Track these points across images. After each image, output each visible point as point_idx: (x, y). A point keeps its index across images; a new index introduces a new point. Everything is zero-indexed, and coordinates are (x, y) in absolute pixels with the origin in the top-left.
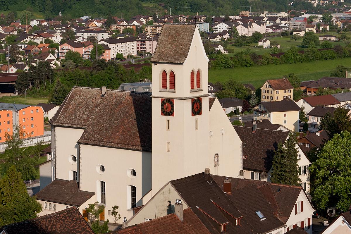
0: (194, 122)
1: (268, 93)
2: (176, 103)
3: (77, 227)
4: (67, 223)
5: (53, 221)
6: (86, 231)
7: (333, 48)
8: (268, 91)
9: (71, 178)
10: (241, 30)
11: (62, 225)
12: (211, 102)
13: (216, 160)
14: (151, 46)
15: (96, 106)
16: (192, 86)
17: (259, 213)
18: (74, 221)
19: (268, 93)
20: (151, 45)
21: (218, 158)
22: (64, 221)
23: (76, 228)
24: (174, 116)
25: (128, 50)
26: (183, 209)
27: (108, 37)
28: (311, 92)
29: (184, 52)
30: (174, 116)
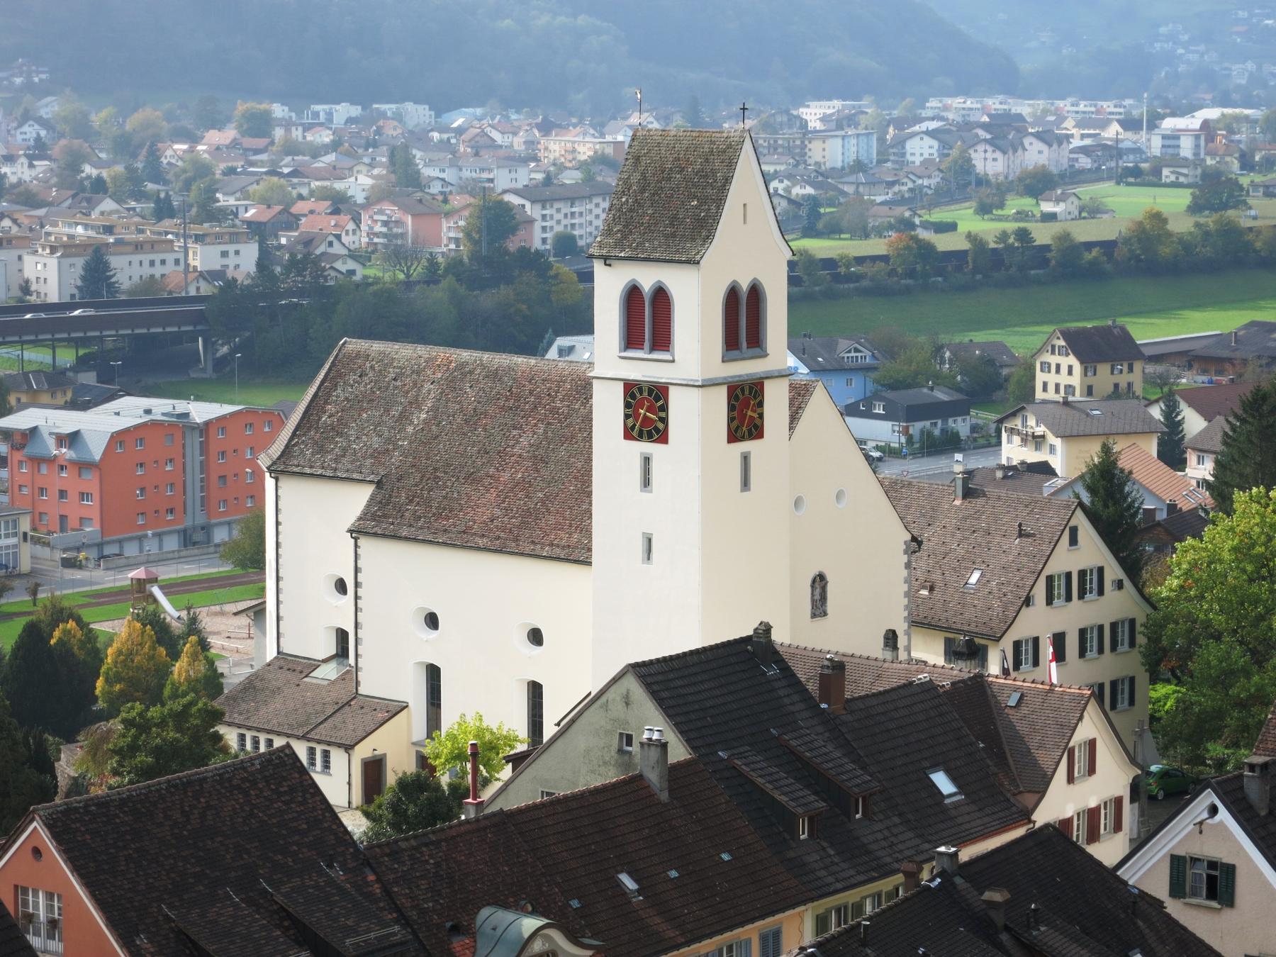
2: (676, 398)
3: (290, 816)
4: (258, 801)
5: (207, 795)
11: (237, 806)
13: (817, 597)
23: (290, 819)
27: (531, 179)
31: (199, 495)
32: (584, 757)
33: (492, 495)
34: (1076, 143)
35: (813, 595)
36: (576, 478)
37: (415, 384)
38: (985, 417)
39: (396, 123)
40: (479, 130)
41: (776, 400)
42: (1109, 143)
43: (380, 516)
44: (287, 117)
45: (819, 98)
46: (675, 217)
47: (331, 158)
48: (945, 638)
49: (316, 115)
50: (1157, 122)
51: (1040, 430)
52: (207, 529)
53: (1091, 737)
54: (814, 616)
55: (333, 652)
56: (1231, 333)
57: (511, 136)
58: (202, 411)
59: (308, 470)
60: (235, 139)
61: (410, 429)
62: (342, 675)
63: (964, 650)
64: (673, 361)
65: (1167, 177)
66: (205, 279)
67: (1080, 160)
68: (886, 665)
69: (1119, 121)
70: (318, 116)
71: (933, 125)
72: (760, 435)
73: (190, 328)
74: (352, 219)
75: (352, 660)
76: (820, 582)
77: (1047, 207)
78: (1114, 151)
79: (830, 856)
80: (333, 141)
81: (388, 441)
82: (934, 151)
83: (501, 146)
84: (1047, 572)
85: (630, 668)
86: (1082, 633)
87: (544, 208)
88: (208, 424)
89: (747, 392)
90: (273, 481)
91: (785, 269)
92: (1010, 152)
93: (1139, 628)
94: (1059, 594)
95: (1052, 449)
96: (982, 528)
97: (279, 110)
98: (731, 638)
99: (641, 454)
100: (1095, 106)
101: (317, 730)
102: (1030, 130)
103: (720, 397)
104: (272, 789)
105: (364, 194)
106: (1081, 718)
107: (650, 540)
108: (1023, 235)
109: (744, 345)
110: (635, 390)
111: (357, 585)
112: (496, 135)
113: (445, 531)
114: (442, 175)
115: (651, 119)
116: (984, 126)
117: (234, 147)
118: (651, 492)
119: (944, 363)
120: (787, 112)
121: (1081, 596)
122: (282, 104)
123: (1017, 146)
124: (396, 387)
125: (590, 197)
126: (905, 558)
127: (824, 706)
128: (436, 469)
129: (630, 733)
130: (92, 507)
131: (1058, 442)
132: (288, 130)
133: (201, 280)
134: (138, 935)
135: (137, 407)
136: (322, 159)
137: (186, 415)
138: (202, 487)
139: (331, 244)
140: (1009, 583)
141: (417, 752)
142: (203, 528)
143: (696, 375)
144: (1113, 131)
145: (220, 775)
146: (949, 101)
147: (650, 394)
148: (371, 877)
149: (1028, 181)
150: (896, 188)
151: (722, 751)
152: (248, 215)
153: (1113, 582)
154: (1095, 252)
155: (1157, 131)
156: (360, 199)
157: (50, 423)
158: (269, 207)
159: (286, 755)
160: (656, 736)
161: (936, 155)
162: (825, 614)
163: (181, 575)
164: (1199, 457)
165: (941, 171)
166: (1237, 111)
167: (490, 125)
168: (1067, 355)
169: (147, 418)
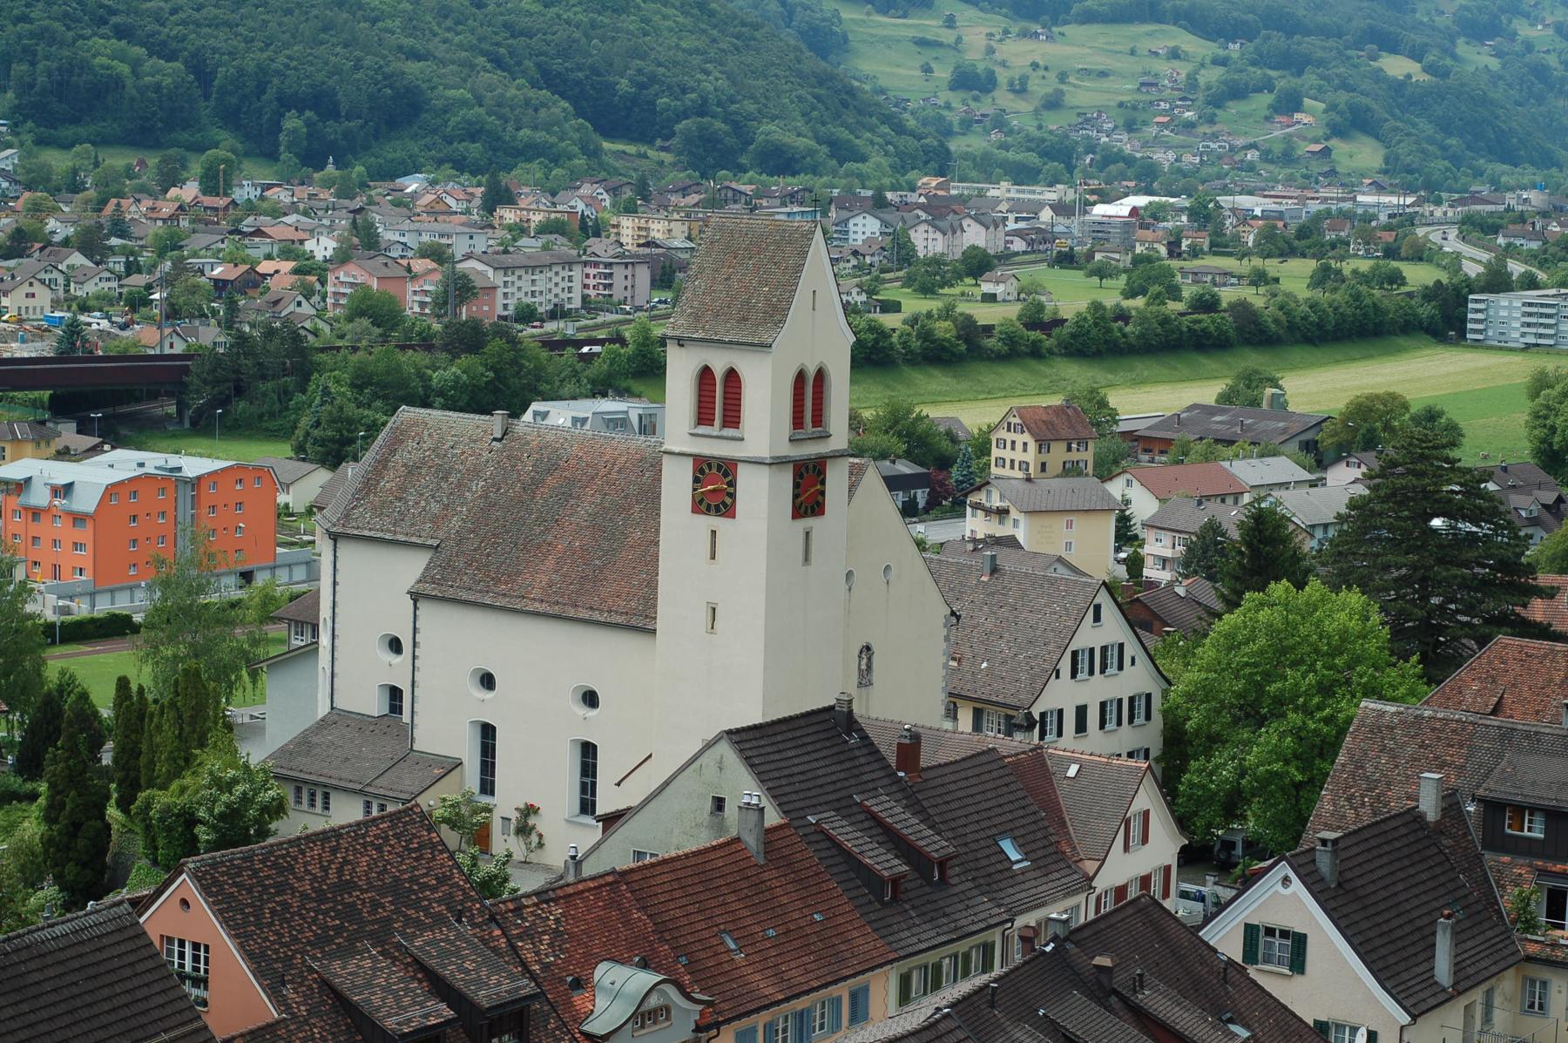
0: (802, 536)
1: (1013, 448)
2: (745, 476)
6: (451, 886)
7: (1225, 311)
8: (1013, 442)
9: (375, 705)
10: (926, 242)
12: (856, 474)
13: (864, 667)
14: (629, 283)
15: (476, 472)
16: (798, 422)
17: (1007, 846)
18: (415, 850)
19: (1013, 448)
21: (869, 659)
22: (379, 849)
24: (734, 517)
25: (554, 292)
28: (1151, 451)
29: (775, 308)
30: (734, 517)
41: (836, 479)
42: (1043, 227)
48: (974, 708)
58: (194, 465)
68: (948, 735)
72: (821, 512)
75: (406, 717)
77: (987, 288)
78: (1046, 236)
79: (912, 918)
81: (446, 507)
84: (1072, 647)
86: (1103, 705)
88: (199, 478)
103: (786, 479)
107: (714, 609)
111: (415, 644)
114: (402, 239)
115: (601, 190)
116: (922, 207)
121: (1103, 671)
123: (956, 229)
125: (550, 266)
126: (945, 631)
127: (901, 774)
130: (85, 557)
131: (1021, 518)
134: (284, 986)
135: (129, 460)
137: (179, 469)
139: (299, 304)
143: (764, 452)
144: (1046, 215)
147: (719, 470)
148: (498, 932)
152: (216, 272)
157: (46, 474)
158: (236, 265)
160: (755, 801)
166: (1164, 199)
168: (1023, 432)
169: (141, 471)
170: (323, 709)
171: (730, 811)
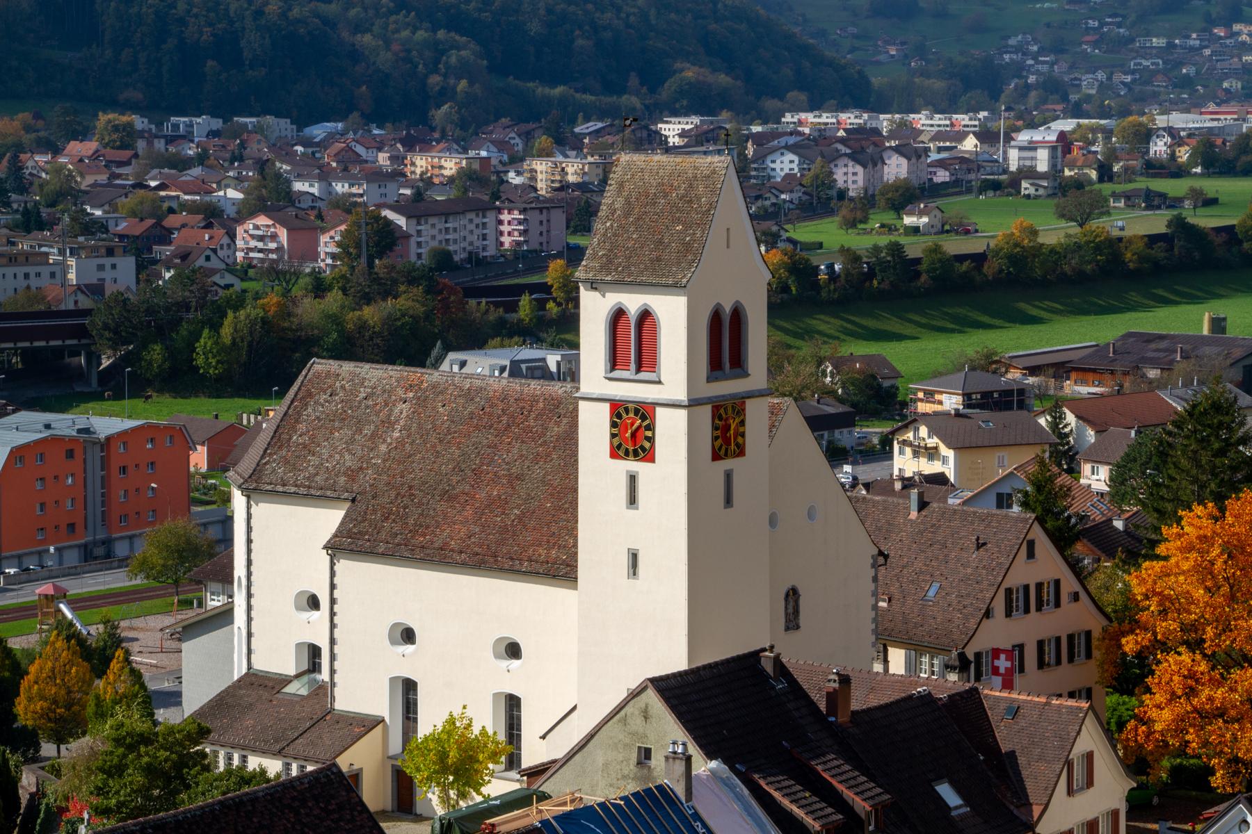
13: (790, 610)
17: (947, 792)
20: (545, 222)
26: (345, 762)
31: (99, 509)
32: (603, 771)
33: (469, 512)
34: (934, 156)
35: (786, 608)
36: (552, 495)
37: (386, 405)
38: (874, 431)
39: (259, 137)
40: (344, 145)
41: (756, 414)
43: (356, 534)
44: (146, 129)
45: (675, 113)
46: (660, 242)
47: (197, 171)
49: (175, 126)
50: (1014, 135)
51: (933, 441)
52: (108, 543)
53: (1088, 750)
54: (787, 629)
55: (305, 667)
56: (1108, 344)
57: (375, 150)
59: (280, 489)
60: (97, 151)
61: (383, 448)
62: (315, 690)
63: (957, 663)
64: (659, 382)
65: (1026, 189)
66: (83, 292)
67: (938, 174)
69: (975, 133)
70: (179, 128)
71: (792, 140)
73: (75, 342)
74: (227, 233)
75: (325, 676)
76: (793, 595)
80: (198, 154)
82: (795, 166)
83: (366, 161)
85: (650, 684)
86: (1041, 644)
87: (419, 223)
89: (730, 411)
90: (244, 499)
91: (766, 287)
92: (870, 166)
93: (1095, 643)
94: (1017, 606)
95: (945, 460)
96: (938, 541)
97: (139, 122)
98: (740, 653)
99: (627, 471)
100: (950, 119)
101: (292, 746)
102: (887, 144)
104: (321, 808)
105: (235, 208)
106: (1079, 733)
108: (896, 249)
109: (727, 365)
110: (622, 410)
111: (333, 601)
112: (360, 149)
113: (423, 547)
116: (842, 141)
117: (96, 158)
118: (637, 509)
119: (826, 377)
120: (646, 127)
121: (1039, 609)
122: (141, 116)
124: (367, 407)
125: (463, 213)
128: (411, 488)
129: (649, 746)
132: (150, 143)
133: (79, 293)
136: (188, 172)
137: (86, 431)
138: (103, 501)
139: (208, 258)
140: (968, 595)
141: (393, 766)
142: (103, 543)
145: (271, 795)
146: (803, 116)
149: (890, 195)
150: (759, 203)
151: (740, 763)
152: (119, 228)
153: (1069, 594)
154: (965, 266)
155: (1013, 143)
156: (231, 211)
159: (333, 773)
161: (796, 170)
162: (798, 627)
163: (85, 590)
164: (1093, 467)
165: (803, 186)
167: (354, 140)
170: (239, 670)
171: (657, 761)
